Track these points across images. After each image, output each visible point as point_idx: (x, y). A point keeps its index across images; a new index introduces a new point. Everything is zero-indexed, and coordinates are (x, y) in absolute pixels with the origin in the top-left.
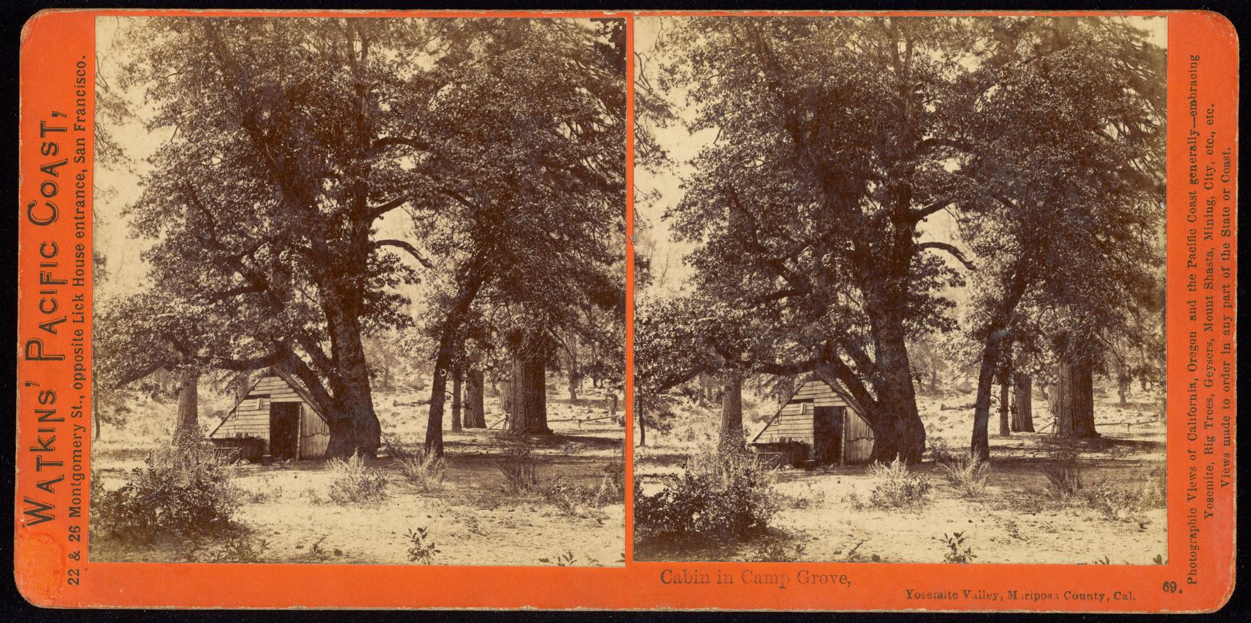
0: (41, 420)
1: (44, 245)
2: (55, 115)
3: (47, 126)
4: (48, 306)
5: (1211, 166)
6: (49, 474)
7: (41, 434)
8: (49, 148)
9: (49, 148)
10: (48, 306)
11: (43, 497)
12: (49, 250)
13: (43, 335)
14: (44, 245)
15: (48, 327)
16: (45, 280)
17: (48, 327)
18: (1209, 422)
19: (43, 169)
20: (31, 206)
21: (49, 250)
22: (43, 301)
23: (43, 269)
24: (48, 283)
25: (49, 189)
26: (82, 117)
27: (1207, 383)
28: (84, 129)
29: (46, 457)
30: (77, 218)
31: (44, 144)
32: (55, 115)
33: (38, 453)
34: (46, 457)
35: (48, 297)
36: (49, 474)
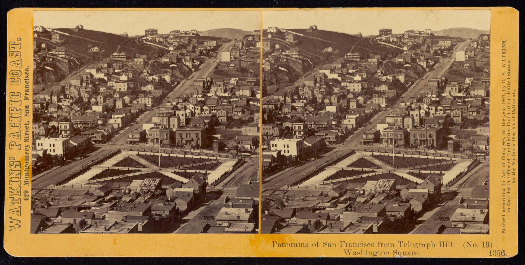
26: (28, 93)
28: (28, 99)
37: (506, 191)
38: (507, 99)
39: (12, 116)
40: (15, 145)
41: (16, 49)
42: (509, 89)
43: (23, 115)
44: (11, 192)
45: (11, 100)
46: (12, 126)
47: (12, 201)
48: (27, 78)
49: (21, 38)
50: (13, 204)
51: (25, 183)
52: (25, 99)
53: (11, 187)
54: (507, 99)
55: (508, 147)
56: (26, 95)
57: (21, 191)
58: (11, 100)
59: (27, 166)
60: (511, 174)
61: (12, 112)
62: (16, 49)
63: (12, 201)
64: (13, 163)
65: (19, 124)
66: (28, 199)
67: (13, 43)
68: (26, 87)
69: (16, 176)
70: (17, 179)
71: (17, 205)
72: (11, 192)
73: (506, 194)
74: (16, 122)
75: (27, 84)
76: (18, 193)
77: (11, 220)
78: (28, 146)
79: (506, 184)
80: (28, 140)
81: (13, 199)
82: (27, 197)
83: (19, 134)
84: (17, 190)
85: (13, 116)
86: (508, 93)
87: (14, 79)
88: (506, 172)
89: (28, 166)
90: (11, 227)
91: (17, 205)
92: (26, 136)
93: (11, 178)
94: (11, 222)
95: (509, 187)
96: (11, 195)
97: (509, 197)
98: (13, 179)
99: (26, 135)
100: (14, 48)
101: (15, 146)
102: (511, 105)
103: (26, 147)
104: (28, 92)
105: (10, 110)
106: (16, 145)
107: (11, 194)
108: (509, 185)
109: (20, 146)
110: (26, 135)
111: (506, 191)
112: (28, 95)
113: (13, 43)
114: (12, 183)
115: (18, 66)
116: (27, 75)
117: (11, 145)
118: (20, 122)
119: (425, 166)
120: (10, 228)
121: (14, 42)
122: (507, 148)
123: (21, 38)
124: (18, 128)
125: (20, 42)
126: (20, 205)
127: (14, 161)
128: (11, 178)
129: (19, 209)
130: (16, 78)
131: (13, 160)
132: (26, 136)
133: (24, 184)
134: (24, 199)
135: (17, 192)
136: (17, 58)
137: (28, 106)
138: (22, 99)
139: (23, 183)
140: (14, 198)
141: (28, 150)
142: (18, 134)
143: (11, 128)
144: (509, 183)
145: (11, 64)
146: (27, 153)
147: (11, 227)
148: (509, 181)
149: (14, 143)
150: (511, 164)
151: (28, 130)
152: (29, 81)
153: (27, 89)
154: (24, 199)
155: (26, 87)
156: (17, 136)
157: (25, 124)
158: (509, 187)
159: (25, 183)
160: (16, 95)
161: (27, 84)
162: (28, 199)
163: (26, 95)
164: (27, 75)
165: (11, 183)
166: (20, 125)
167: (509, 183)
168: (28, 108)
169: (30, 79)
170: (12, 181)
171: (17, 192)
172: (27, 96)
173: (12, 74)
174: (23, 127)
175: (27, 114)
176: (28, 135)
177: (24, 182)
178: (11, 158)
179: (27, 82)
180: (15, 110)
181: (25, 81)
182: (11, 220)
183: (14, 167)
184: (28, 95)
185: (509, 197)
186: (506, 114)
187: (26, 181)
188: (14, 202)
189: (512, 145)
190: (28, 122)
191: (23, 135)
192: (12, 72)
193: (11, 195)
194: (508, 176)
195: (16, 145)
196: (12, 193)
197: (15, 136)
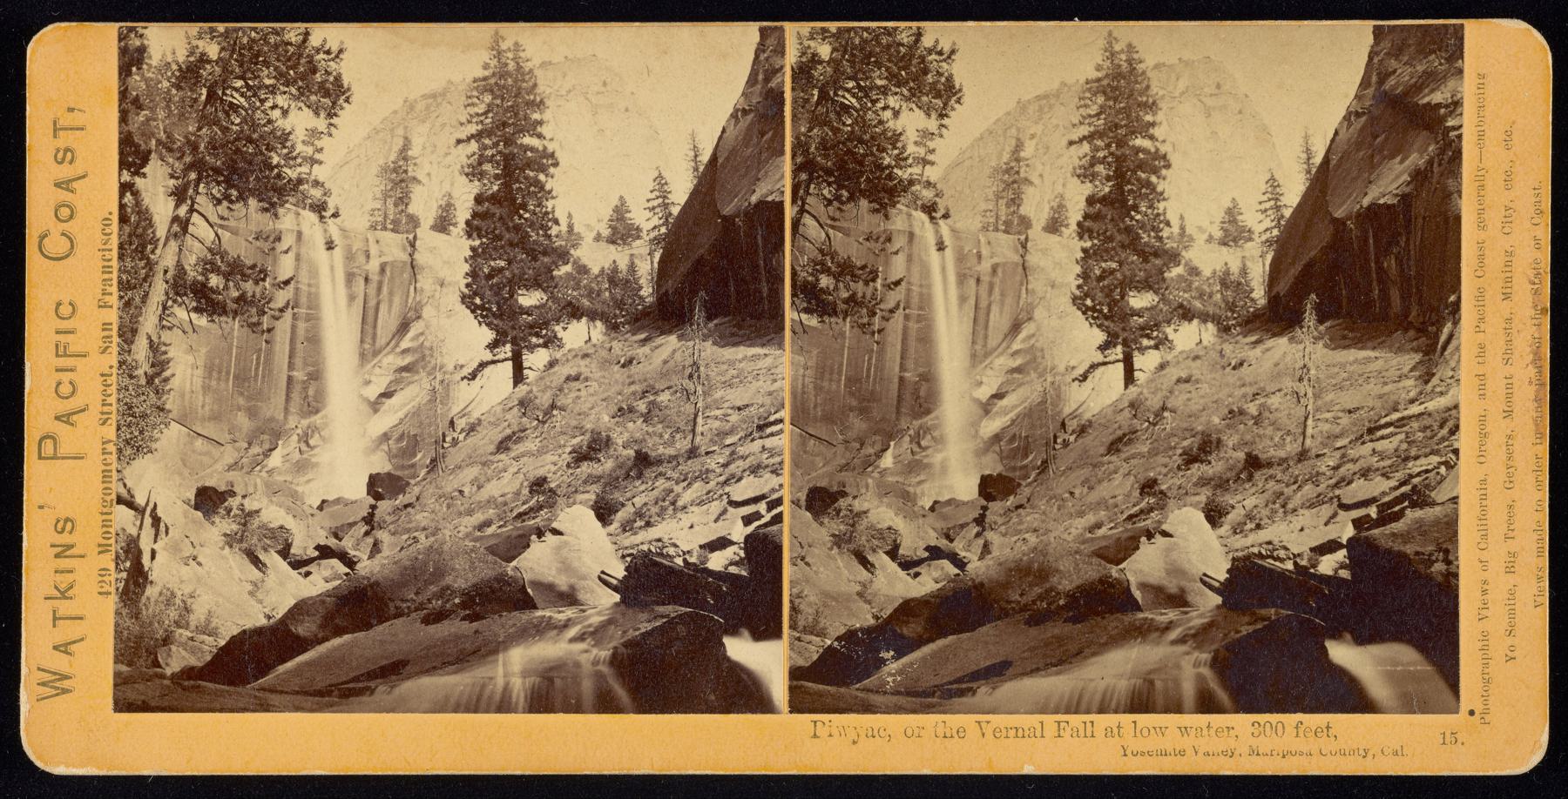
0: (57, 556)
1: (59, 304)
2: (71, 110)
3: (61, 123)
4: (65, 389)
5: (1511, 205)
6: (67, 631)
7: (59, 577)
8: (65, 154)
9: (65, 154)
10: (65, 389)
11: (60, 663)
12: (65, 310)
13: (61, 429)
14: (59, 304)
15: (65, 418)
16: (61, 351)
17: (65, 418)
18: (1511, 534)
19: (58, 185)
20: (43, 237)
21: (65, 310)
22: (59, 384)
23: (61, 337)
24: (65, 355)
25: (65, 212)
27: (1508, 485)
29: (65, 607)
30: (102, 514)
31: (58, 151)
32: (71, 110)
33: (56, 603)
34: (65, 607)
35: (66, 377)
36: (67, 631)
51: (100, 549)
99: (103, 405)
103: (103, 443)
110: (103, 405)
161: (106, 264)
163: (103, 294)
181: (101, 253)
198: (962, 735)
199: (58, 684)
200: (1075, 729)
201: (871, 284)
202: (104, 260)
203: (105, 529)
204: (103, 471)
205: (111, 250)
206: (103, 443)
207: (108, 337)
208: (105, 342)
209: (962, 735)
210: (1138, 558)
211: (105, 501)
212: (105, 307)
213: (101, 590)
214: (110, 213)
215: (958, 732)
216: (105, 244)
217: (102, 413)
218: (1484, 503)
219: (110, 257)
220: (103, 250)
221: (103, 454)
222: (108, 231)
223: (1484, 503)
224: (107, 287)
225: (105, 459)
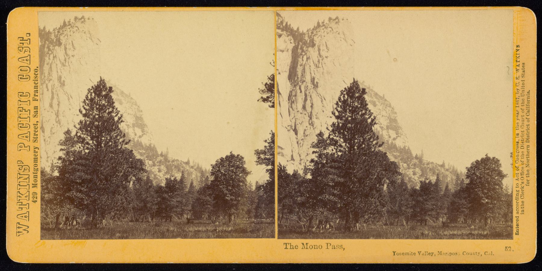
26: (37, 94)
28: (37, 100)
30: (34, 173)
37: (520, 193)
38: (520, 102)
39: (19, 185)
40: (23, 146)
41: (25, 45)
42: (523, 91)
43: (31, 116)
44: (19, 197)
45: (20, 101)
46: (21, 127)
47: (21, 42)
48: (36, 79)
49: (29, 34)
50: (21, 209)
51: (33, 186)
52: (33, 100)
53: (19, 192)
54: (520, 102)
55: (522, 150)
56: (34, 96)
57: (29, 217)
58: (20, 101)
59: (36, 168)
60: (525, 176)
61: (21, 113)
62: (25, 45)
63: (21, 42)
64: (21, 167)
65: (28, 76)
66: (36, 201)
67: (22, 39)
68: (35, 88)
69: (24, 181)
70: (26, 184)
71: (24, 211)
72: (19, 197)
73: (519, 196)
74: (24, 123)
75: (36, 85)
76: (26, 198)
77: (18, 225)
78: (37, 148)
79: (520, 187)
80: (37, 141)
81: (21, 204)
82: (35, 199)
83: (28, 135)
84: (25, 195)
85: (21, 116)
86: (522, 95)
87: (23, 76)
88: (520, 174)
89: (37, 169)
90: (19, 232)
91: (24, 211)
92: (35, 137)
93: (20, 182)
94: (19, 228)
95: (523, 189)
96: (19, 200)
97: (522, 200)
98: (21, 184)
99: (34, 135)
100: (23, 43)
101: (23, 148)
102: (524, 107)
103: (34, 149)
104: (37, 93)
105: (19, 111)
106: (25, 147)
107: (19, 198)
108: (523, 187)
109: (28, 147)
110: (34, 135)
111: (520, 193)
112: (37, 96)
113: (22, 39)
114: (21, 187)
115: (26, 218)
116: (35, 76)
117: (20, 147)
118: (29, 66)
119: (464, 232)
120: (18, 234)
121: (23, 38)
122: (520, 150)
123: (29, 34)
124: (27, 97)
125: (29, 38)
126: (28, 210)
127: (23, 165)
128: (20, 182)
129: (27, 215)
130: (25, 75)
131: (21, 164)
132: (35, 137)
133: (33, 187)
134: (32, 201)
135: (25, 197)
136: (27, 54)
137: (37, 107)
138: (31, 99)
139: (31, 186)
140: (22, 203)
141: (37, 152)
142: (25, 215)
143: (20, 129)
144: (523, 185)
145: (18, 216)
146: (36, 155)
147: (19, 232)
148: (523, 183)
149: (22, 145)
150: (524, 166)
151: (36, 131)
152: (38, 82)
153: (36, 89)
154: (32, 201)
155: (35, 88)
156: (26, 137)
157: (34, 125)
158: (523, 189)
159: (33, 186)
160: (24, 95)
161: (36, 85)
162: (36, 201)
163: (34, 96)
164: (35, 76)
165: (19, 187)
166: (29, 126)
167: (523, 185)
168: (37, 162)
169: (38, 79)
170: (20, 186)
171: (25, 197)
172: (36, 97)
173: (21, 70)
174: (32, 127)
175: (36, 115)
176: (37, 135)
177: (33, 184)
178: (19, 162)
179: (36, 83)
180: (24, 111)
181: (34, 81)
182: (18, 225)
183: (23, 170)
184: (37, 96)
185: (522, 200)
186: (520, 117)
187: (34, 183)
188: (23, 42)
189: (525, 146)
190: (37, 122)
191: (32, 136)
192: (21, 68)
193: (19, 200)
194: (522, 179)
195: (25, 147)
196: (20, 198)
197: (22, 217)
198: (297, 248)
199: (22, 229)
200: (333, 246)
201: (503, 190)
202: (35, 156)
203: (35, 163)
204: (34, 158)
205: (37, 80)
206: (34, 149)
207: (36, 91)
208: (35, 113)
209: (297, 248)
210: (361, 82)
211: (35, 169)
212: (35, 100)
213: (33, 200)
214: (37, 67)
215: (295, 247)
216: (35, 78)
217: (34, 138)
218: (529, 100)
219: (37, 74)
220: (35, 80)
221: (34, 152)
222: (36, 74)
223: (529, 100)
224: (36, 93)
225: (35, 154)
